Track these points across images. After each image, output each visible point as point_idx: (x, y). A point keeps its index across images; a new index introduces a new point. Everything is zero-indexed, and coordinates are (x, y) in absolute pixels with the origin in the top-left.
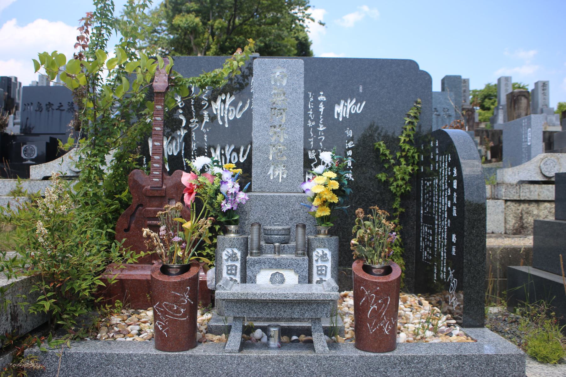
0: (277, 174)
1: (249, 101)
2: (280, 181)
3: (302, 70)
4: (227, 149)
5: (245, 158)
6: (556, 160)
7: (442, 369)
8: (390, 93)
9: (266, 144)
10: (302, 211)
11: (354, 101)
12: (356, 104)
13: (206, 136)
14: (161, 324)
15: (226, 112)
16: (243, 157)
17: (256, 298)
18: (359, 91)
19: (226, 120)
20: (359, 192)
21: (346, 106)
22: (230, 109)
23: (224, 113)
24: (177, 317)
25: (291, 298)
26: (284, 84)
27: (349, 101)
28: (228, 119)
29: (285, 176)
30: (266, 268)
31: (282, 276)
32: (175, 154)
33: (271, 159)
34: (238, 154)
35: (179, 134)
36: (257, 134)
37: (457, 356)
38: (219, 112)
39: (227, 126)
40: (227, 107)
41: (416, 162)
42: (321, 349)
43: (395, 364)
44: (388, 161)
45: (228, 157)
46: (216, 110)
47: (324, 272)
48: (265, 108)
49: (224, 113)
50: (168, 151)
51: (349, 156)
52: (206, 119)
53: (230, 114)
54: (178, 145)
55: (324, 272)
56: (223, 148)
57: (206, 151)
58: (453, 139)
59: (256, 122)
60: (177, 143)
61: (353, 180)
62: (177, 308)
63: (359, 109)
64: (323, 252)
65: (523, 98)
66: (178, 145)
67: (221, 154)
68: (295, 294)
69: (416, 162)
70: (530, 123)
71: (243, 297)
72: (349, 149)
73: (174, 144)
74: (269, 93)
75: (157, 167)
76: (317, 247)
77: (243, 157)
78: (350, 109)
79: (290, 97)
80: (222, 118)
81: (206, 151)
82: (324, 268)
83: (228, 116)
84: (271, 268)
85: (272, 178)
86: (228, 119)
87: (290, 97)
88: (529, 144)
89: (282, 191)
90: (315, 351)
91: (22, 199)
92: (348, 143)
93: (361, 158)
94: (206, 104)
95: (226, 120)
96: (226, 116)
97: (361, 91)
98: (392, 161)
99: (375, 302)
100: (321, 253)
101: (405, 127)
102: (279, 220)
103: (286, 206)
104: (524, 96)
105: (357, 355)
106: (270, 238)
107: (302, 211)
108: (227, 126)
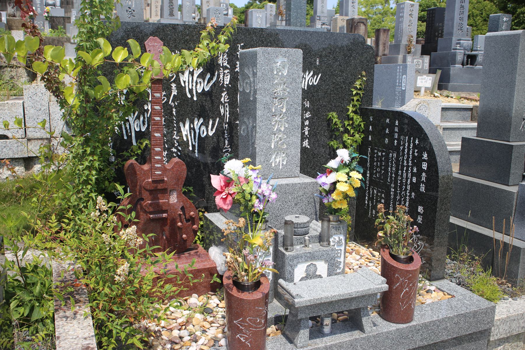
0: (278, 162)
1: (216, 73)
2: (281, 168)
3: (301, 60)
4: (196, 123)
5: (214, 131)
6: (427, 106)
7: (447, 327)
8: (341, 66)
9: (269, 133)
10: (305, 196)
11: (312, 73)
12: (313, 76)
13: (174, 110)
14: (244, 337)
15: (194, 84)
16: (212, 130)
17: (328, 300)
18: (316, 64)
19: (195, 93)
20: (314, 158)
21: (305, 78)
22: (198, 81)
23: (192, 85)
24: (259, 328)
25: (354, 296)
26: (285, 74)
27: (307, 73)
28: (197, 91)
29: (285, 163)
30: (302, 262)
31: (315, 266)
32: (143, 130)
33: (273, 147)
34: (207, 127)
35: (146, 108)
36: (261, 124)
37: (457, 316)
38: (187, 84)
39: (195, 99)
40: (195, 79)
41: (361, 131)
42: (369, 330)
43: (419, 330)
44: (338, 129)
45: (197, 131)
46: (184, 82)
47: (339, 255)
48: (268, 98)
49: (192, 85)
50: (136, 126)
51: (307, 126)
52: (174, 92)
53: (199, 85)
54: (146, 120)
55: (339, 255)
56: (192, 122)
57: (175, 125)
58: (427, 131)
59: (260, 112)
60: (144, 118)
61: (309, 147)
62: (260, 321)
63: (315, 82)
64: (339, 238)
65: (362, 25)
66: (146, 120)
67: (190, 128)
68: (358, 292)
69: (361, 131)
70: (406, 71)
71: (318, 302)
72: (307, 119)
73: (142, 118)
74: (271, 82)
75: (159, 159)
76: (334, 234)
77: (212, 130)
78: (308, 80)
79: (290, 86)
80: (191, 91)
81: (175, 125)
82: (339, 251)
83: (196, 89)
84: (306, 261)
85: (273, 165)
86: (197, 91)
87: (290, 86)
88: (403, 89)
89: (282, 176)
90: (364, 332)
91: (218, 280)
92: (306, 113)
93: (316, 128)
94: (173, 76)
95: (195, 93)
96: (194, 88)
97: (318, 63)
98: (341, 129)
99: (408, 286)
100: (337, 239)
101: (352, 98)
102: (286, 206)
103: (291, 194)
104: (363, 23)
105: (394, 328)
106: (297, 231)
107: (305, 196)
108: (195, 99)
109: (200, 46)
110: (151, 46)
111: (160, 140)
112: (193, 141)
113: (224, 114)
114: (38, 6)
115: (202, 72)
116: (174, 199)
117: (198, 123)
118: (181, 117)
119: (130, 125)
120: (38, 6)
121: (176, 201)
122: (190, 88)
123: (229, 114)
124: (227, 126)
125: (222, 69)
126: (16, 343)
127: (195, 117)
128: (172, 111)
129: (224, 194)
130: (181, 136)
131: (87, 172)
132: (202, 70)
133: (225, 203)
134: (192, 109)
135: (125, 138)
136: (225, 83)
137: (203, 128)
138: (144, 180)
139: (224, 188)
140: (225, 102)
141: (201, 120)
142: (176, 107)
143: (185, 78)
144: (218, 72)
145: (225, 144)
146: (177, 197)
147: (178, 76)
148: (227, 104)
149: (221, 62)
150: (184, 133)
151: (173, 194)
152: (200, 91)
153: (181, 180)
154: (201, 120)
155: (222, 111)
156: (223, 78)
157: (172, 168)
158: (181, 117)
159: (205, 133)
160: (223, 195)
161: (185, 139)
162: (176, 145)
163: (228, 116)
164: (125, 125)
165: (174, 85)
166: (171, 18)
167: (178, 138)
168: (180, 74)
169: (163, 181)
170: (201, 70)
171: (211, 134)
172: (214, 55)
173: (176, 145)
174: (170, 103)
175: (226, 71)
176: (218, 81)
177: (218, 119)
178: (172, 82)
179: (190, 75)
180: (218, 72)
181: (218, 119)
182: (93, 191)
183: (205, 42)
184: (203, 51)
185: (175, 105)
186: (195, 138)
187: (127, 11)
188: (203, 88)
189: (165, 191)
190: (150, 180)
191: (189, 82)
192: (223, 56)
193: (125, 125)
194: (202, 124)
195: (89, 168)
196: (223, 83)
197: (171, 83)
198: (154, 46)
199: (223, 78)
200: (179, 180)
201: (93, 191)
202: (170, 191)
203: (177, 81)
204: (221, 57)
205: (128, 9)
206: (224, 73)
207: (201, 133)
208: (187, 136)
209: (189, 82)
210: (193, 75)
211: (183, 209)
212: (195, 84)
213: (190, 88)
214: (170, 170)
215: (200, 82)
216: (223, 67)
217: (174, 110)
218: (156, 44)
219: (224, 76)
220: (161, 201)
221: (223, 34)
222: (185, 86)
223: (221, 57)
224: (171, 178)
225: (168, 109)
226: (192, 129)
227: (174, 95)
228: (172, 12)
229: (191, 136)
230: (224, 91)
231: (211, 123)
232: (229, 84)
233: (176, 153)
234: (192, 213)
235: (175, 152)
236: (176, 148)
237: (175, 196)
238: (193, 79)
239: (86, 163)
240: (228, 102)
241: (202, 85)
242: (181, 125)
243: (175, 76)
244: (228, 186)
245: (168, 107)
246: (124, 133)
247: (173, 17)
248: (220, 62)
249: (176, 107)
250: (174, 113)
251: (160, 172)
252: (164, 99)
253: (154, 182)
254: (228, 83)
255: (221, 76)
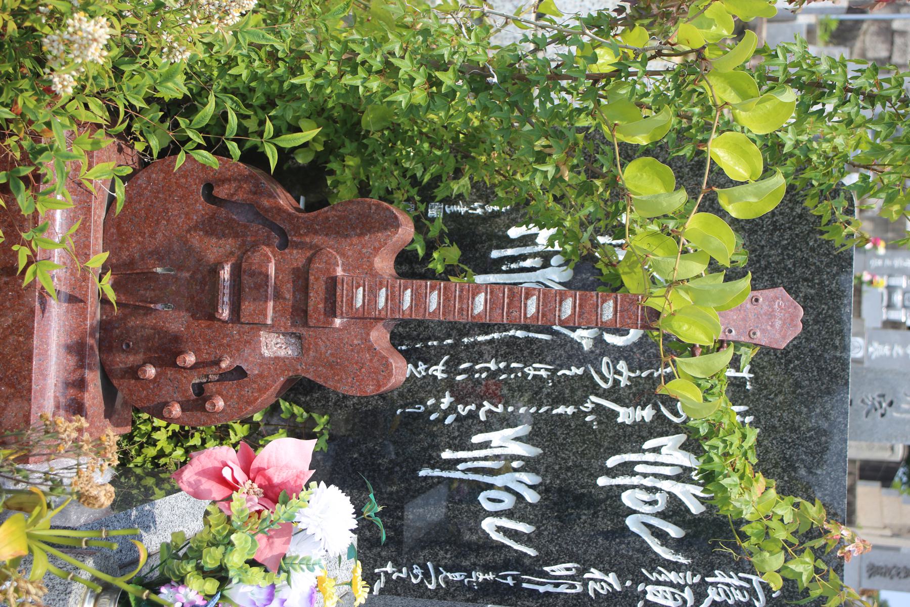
1: (682, 560)
5: (496, 537)
13: (570, 410)
15: (649, 482)
16: (499, 529)
22: (658, 496)
23: (645, 476)
28: (625, 488)
34: (509, 514)
39: (602, 481)
40: (666, 485)
45: (498, 481)
46: (656, 450)
49: (645, 476)
52: (626, 415)
53: (646, 497)
56: (529, 465)
75: (401, 302)
77: (499, 529)
80: (627, 469)
83: (634, 487)
94: (677, 414)
96: (636, 480)
108: (602, 481)
109: (773, 492)
110: (771, 306)
111: (461, 309)
112: (470, 465)
113: (546, 575)
114: (888, 262)
115: (688, 510)
116: (274, 346)
117: (525, 484)
118: (545, 429)
119: (532, 269)
120: (888, 262)
121: (267, 353)
122: (638, 468)
123: (548, 593)
124: (510, 581)
125: (697, 579)
126: (360, 583)
127: (543, 476)
128: (566, 403)
129: (240, 475)
130: (488, 427)
131: (377, 63)
132: (694, 511)
133: (205, 473)
134: (568, 469)
135: (495, 254)
136: (649, 588)
137: (508, 502)
138: (343, 255)
139: (259, 479)
140: (585, 585)
141: (532, 497)
142: (580, 415)
143: (671, 451)
144: (688, 567)
145: (451, 571)
146: (277, 358)
147: (676, 429)
148: (579, 589)
149: (719, 579)
150: (496, 437)
151: (288, 344)
152: (627, 499)
153: (330, 373)
154: (532, 497)
155: (558, 570)
156: (664, 583)
157: (371, 348)
158: (545, 429)
159: (488, 506)
160: (233, 471)
161: (476, 439)
162: (460, 407)
163: (542, 589)
164: (534, 255)
165: (647, 414)
166: (864, 569)
167: (483, 418)
168: (682, 438)
169: (332, 311)
170: (696, 508)
171: (488, 525)
172: (744, 537)
173: (460, 407)
174: (593, 398)
175: (688, 594)
176: (656, 562)
177: (532, 552)
178: (659, 410)
179: (678, 471)
180: (688, 567)
181: (532, 552)
182: (320, 81)
183: (785, 510)
184: (753, 499)
185: (586, 414)
186: (476, 471)
187: (883, 396)
188: (635, 512)
189: (299, 316)
190: (339, 272)
191: (655, 464)
192: (741, 588)
193: (534, 255)
194: (519, 497)
195: (389, 69)
196: (648, 582)
197: (656, 407)
198: (771, 315)
199: (664, 583)
200: (331, 366)
201: (320, 81)
202: (299, 337)
203: (661, 427)
204: (736, 582)
205: (888, 400)
206: (681, 588)
207: (492, 494)
208: (486, 445)
209: (655, 464)
210: (678, 478)
211: (239, 373)
212: (651, 482)
213: (638, 468)
214: (366, 339)
215: (655, 502)
216: (703, 584)
217: (570, 410)
218: (778, 323)
219: (671, 584)
220: (271, 304)
221: (817, 570)
222: (644, 451)
223: (736, 582)
224: (341, 340)
225: (573, 391)
226: (507, 463)
227: (617, 414)
228: (884, 574)
229: (486, 459)
230: (623, 583)
231: (524, 528)
232: (647, 602)
233: (436, 408)
234: (220, 404)
235: (438, 403)
236: (452, 409)
237: (282, 353)
238: (667, 477)
239: (405, 66)
240: (585, 593)
241: (648, 509)
242: (523, 429)
243: (676, 420)
244: (266, 496)
245: (579, 393)
246: (510, 252)
247: (865, 575)
248: (720, 577)
249: (580, 415)
250: (561, 410)
251: (359, 303)
252: (606, 380)
253: (332, 283)
254: (649, 597)
255: (672, 576)
